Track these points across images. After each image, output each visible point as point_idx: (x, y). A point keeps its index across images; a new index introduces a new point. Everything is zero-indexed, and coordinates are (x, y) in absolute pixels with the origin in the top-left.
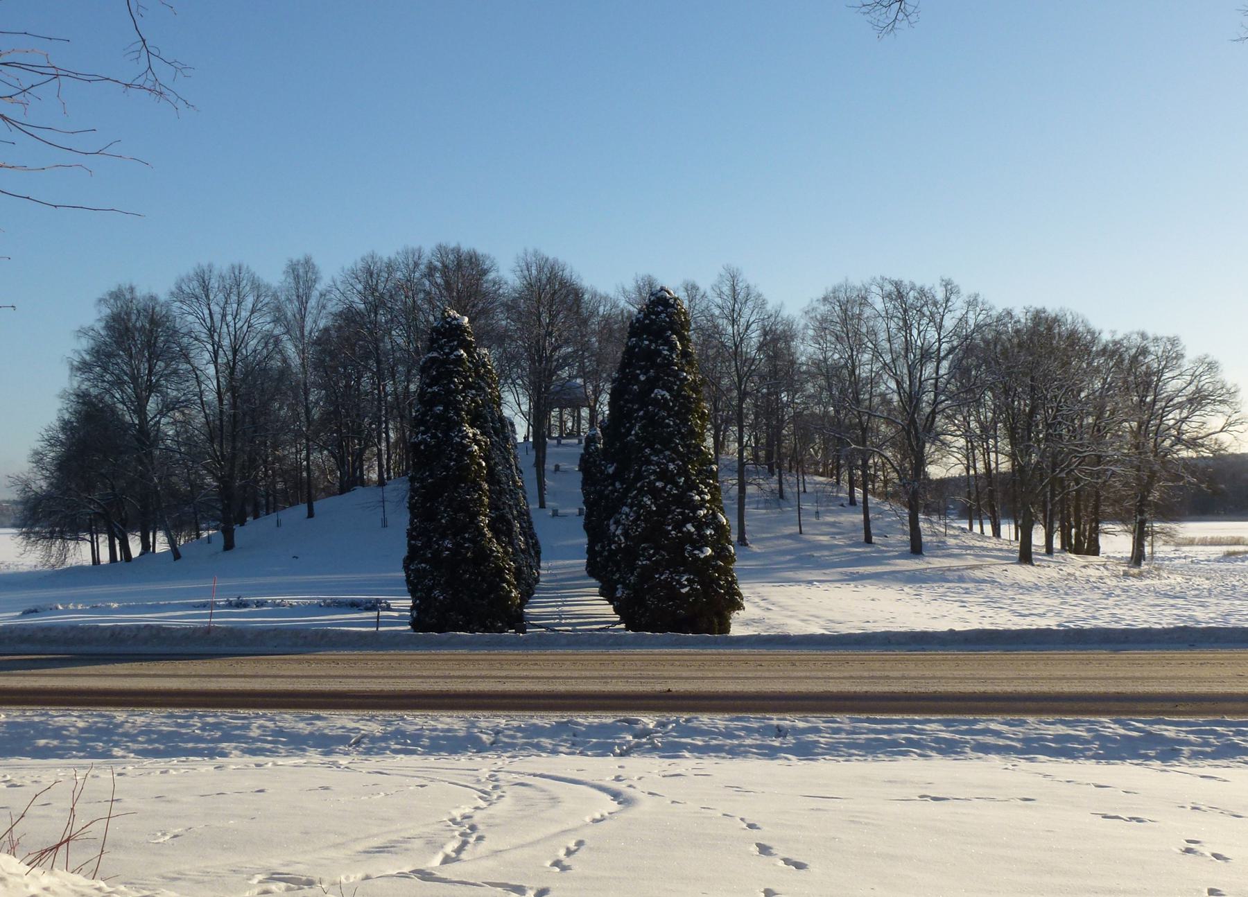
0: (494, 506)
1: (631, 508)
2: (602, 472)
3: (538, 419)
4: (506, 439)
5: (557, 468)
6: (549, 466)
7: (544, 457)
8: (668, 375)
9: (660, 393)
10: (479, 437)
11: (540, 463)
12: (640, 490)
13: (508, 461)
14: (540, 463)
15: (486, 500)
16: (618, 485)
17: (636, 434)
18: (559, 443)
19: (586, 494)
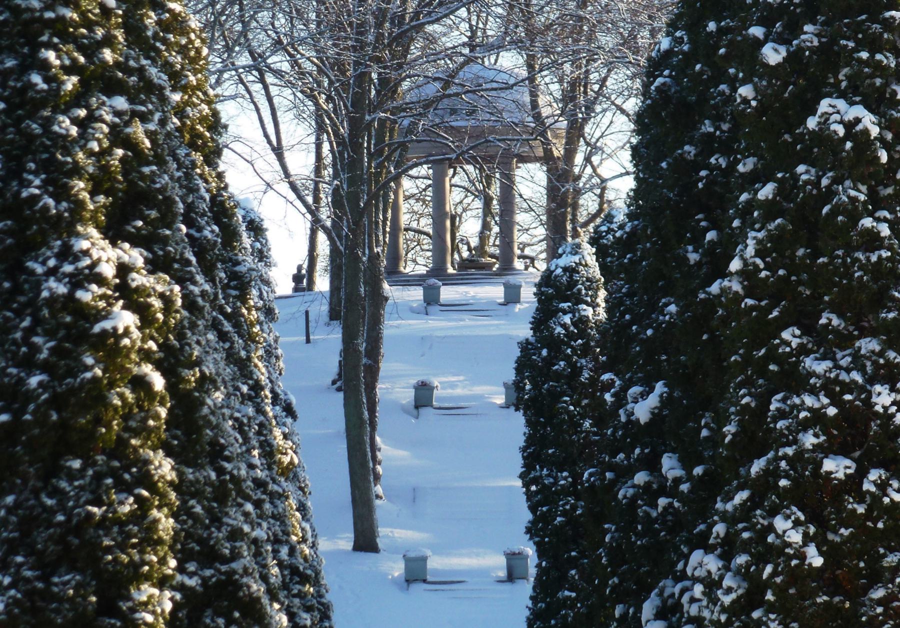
0: (195, 548)
1: (727, 557)
2: (604, 416)
3: (354, 207)
4: (240, 284)
5: (423, 395)
6: (394, 386)
7: (374, 352)
8: (875, 45)
9: (837, 112)
10: (139, 279)
11: (357, 377)
12: (762, 488)
13: (243, 367)
14: (357, 377)
15: (166, 525)
16: (670, 466)
17: (748, 274)
18: (431, 299)
19: (541, 499)
